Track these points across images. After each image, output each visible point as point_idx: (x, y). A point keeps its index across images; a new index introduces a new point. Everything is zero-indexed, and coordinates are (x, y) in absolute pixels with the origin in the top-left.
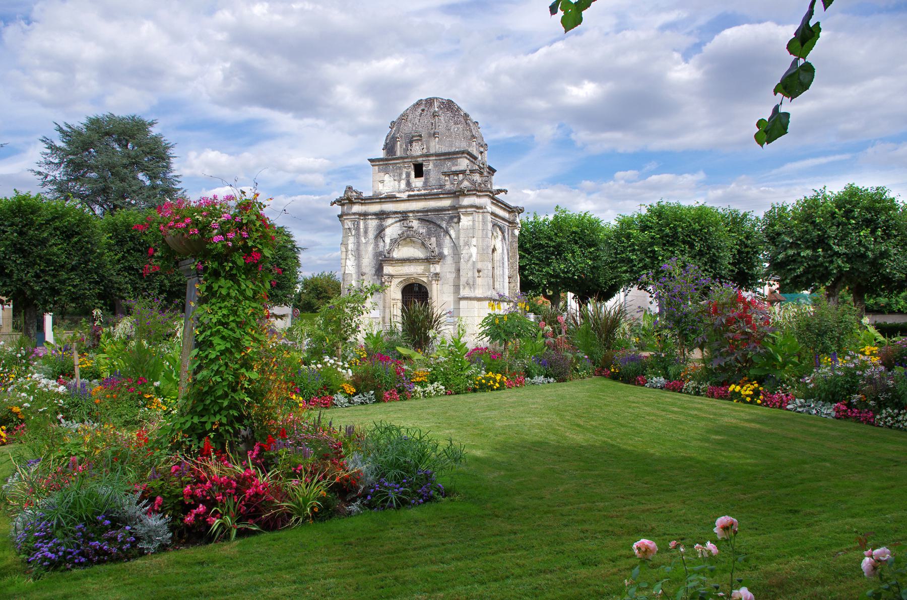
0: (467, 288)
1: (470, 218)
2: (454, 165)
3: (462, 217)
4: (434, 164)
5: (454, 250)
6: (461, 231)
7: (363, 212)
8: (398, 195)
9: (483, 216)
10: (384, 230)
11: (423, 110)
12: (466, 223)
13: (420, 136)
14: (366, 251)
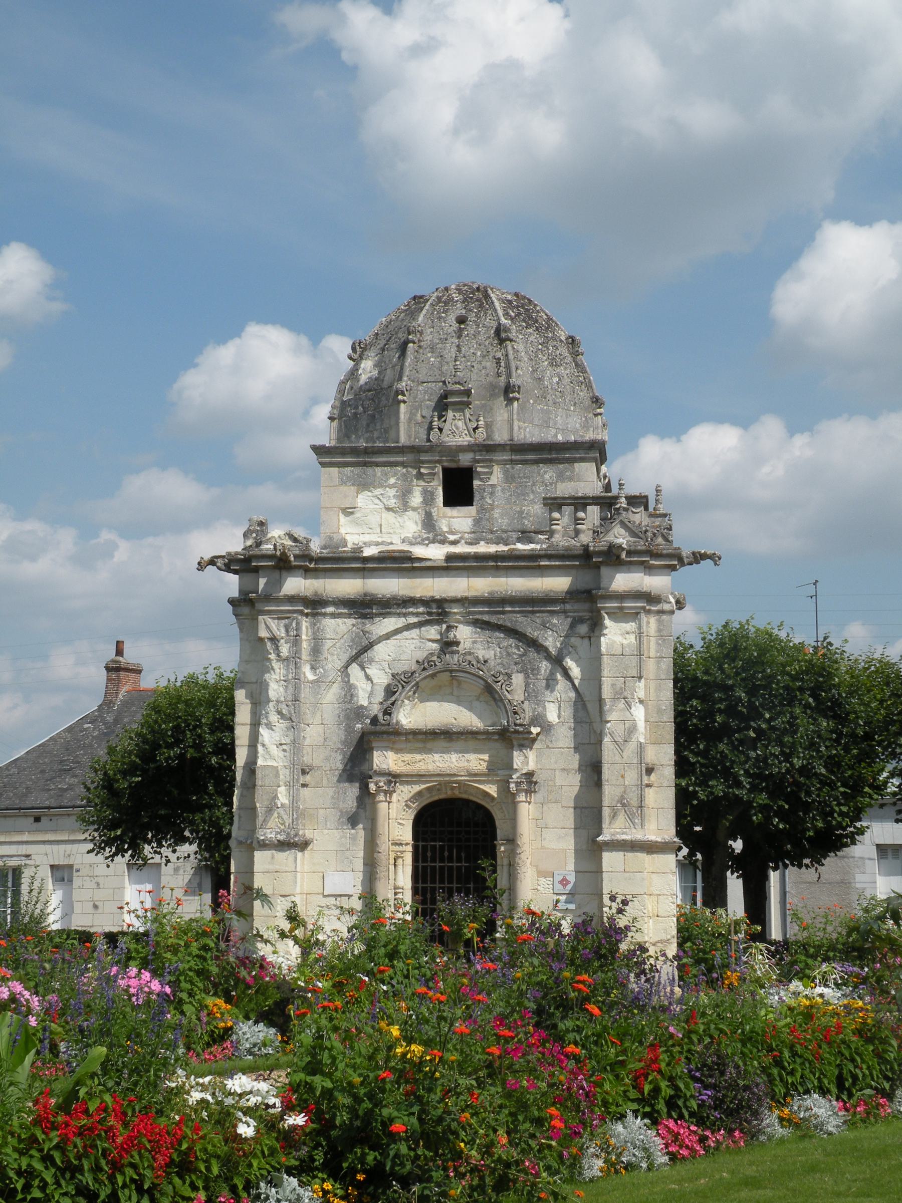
0: (621, 819)
1: (631, 626)
2: (561, 477)
3: (607, 622)
4: (506, 473)
5: (576, 711)
6: (605, 660)
7: (309, 593)
8: (419, 551)
9: (659, 622)
10: (371, 646)
11: (461, 320)
12: (618, 639)
13: (468, 393)
14: (316, 705)
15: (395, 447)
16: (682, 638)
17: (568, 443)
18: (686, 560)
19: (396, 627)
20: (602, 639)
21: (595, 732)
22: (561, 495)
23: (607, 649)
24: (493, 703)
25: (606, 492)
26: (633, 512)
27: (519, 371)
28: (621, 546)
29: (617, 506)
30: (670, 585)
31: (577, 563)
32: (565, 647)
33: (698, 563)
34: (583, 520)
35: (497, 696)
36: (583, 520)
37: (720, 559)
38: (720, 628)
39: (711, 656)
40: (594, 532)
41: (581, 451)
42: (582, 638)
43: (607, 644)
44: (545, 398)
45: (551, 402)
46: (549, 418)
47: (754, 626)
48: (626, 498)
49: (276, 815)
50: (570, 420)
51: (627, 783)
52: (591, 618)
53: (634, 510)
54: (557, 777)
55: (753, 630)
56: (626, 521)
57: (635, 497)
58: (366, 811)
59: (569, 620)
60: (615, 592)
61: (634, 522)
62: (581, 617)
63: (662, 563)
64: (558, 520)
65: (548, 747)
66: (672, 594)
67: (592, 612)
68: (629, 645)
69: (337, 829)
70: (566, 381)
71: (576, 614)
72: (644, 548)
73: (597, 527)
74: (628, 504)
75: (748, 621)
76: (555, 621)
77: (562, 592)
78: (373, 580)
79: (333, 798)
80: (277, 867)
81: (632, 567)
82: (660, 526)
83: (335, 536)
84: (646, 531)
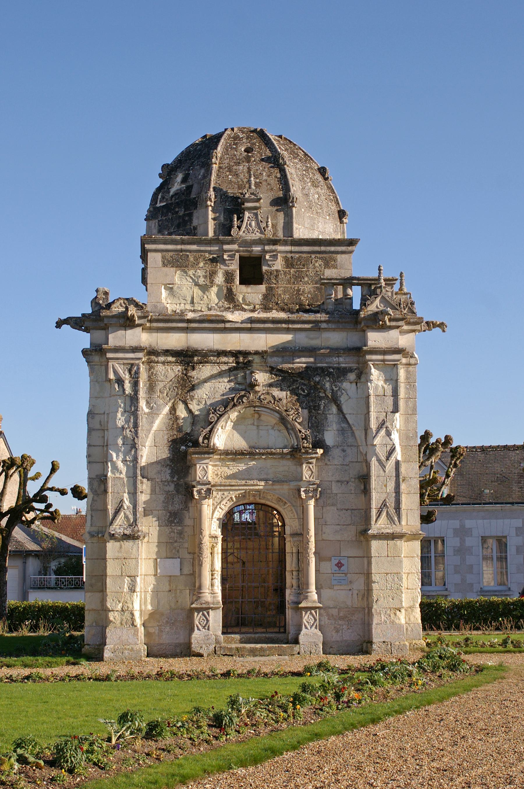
15: (205, 240)
19: (212, 373)
21: (361, 453)
24: (285, 432)
27: (294, 188)
35: (289, 426)
44: (311, 209)
45: (315, 212)
46: (314, 223)
48: (385, 280)
49: (122, 514)
50: (327, 226)
51: (388, 491)
52: (357, 369)
54: (333, 487)
58: (189, 512)
62: (350, 367)
65: (326, 464)
69: (167, 526)
70: (323, 198)
78: (206, 334)
79: (163, 502)
80: (125, 555)
83: (158, 304)
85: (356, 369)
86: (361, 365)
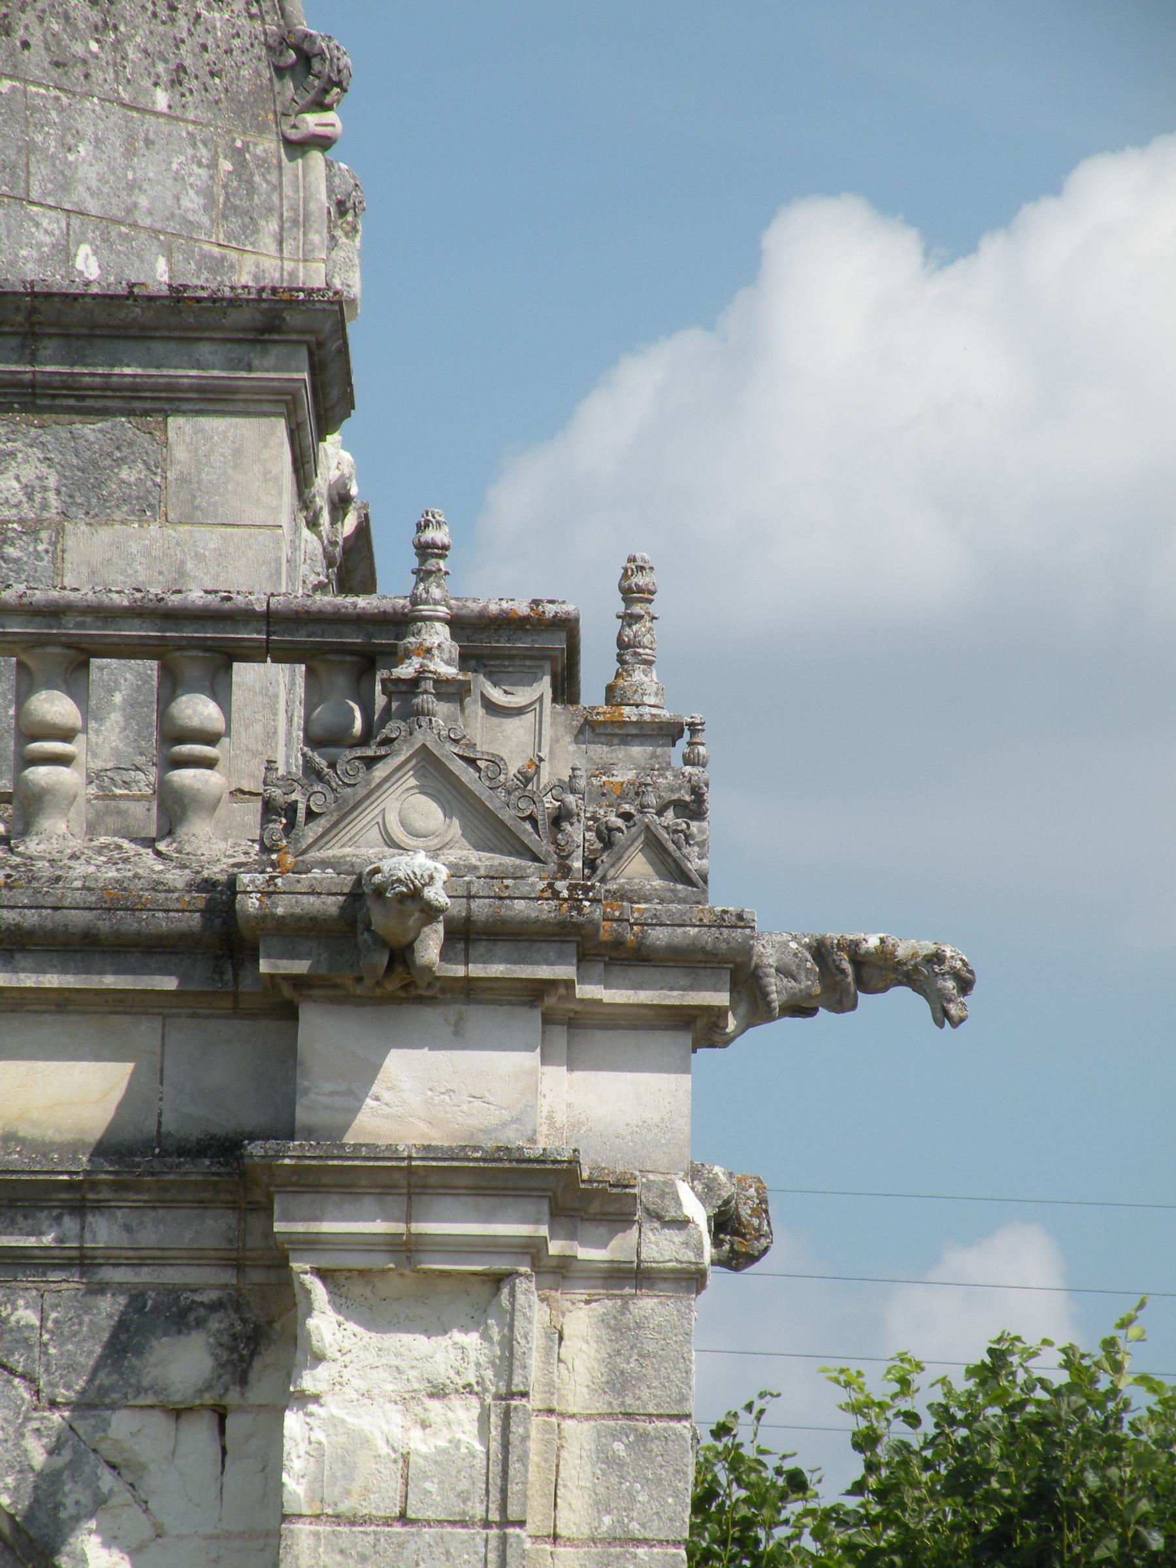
16: (743, 1432)
17: (131, 295)
18: (777, 989)
20: (292, 1421)
22: (87, 595)
23: (317, 1482)
25: (345, 585)
26: (492, 708)
28: (415, 895)
29: (405, 671)
30: (683, 1125)
31: (169, 983)
32: (74, 1466)
33: (842, 1003)
34: (211, 739)
36: (211, 739)
37: (965, 985)
38: (963, 1385)
39: (907, 1546)
40: (269, 809)
41: (204, 350)
42: (178, 1413)
43: (317, 1452)
46: (29, 148)
47: (1144, 1380)
48: (458, 624)
50: (148, 167)
52: (231, 1302)
53: (497, 695)
55: (1142, 1401)
56: (447, 753)
57: (506, 623)
59: (109, 1307)
60: (373, 1150)
61: (496, 762)
62: (173, 1291)
63: (645, 996)
64: (67, 735)
66: (694, 1174)
67: (239, 1266)
68: (443, 1460)
71: (145, 1276)
72: (545, 910)
73: (289, 781)
74: (466, 660)
75: (1110, 1345)
76: (26, 1315)
77: (73, 1147)
81: (478, 1017)
82: (638, 790)
84: (560, 818)
85: (215, 1307)
86: (256, 1276)
